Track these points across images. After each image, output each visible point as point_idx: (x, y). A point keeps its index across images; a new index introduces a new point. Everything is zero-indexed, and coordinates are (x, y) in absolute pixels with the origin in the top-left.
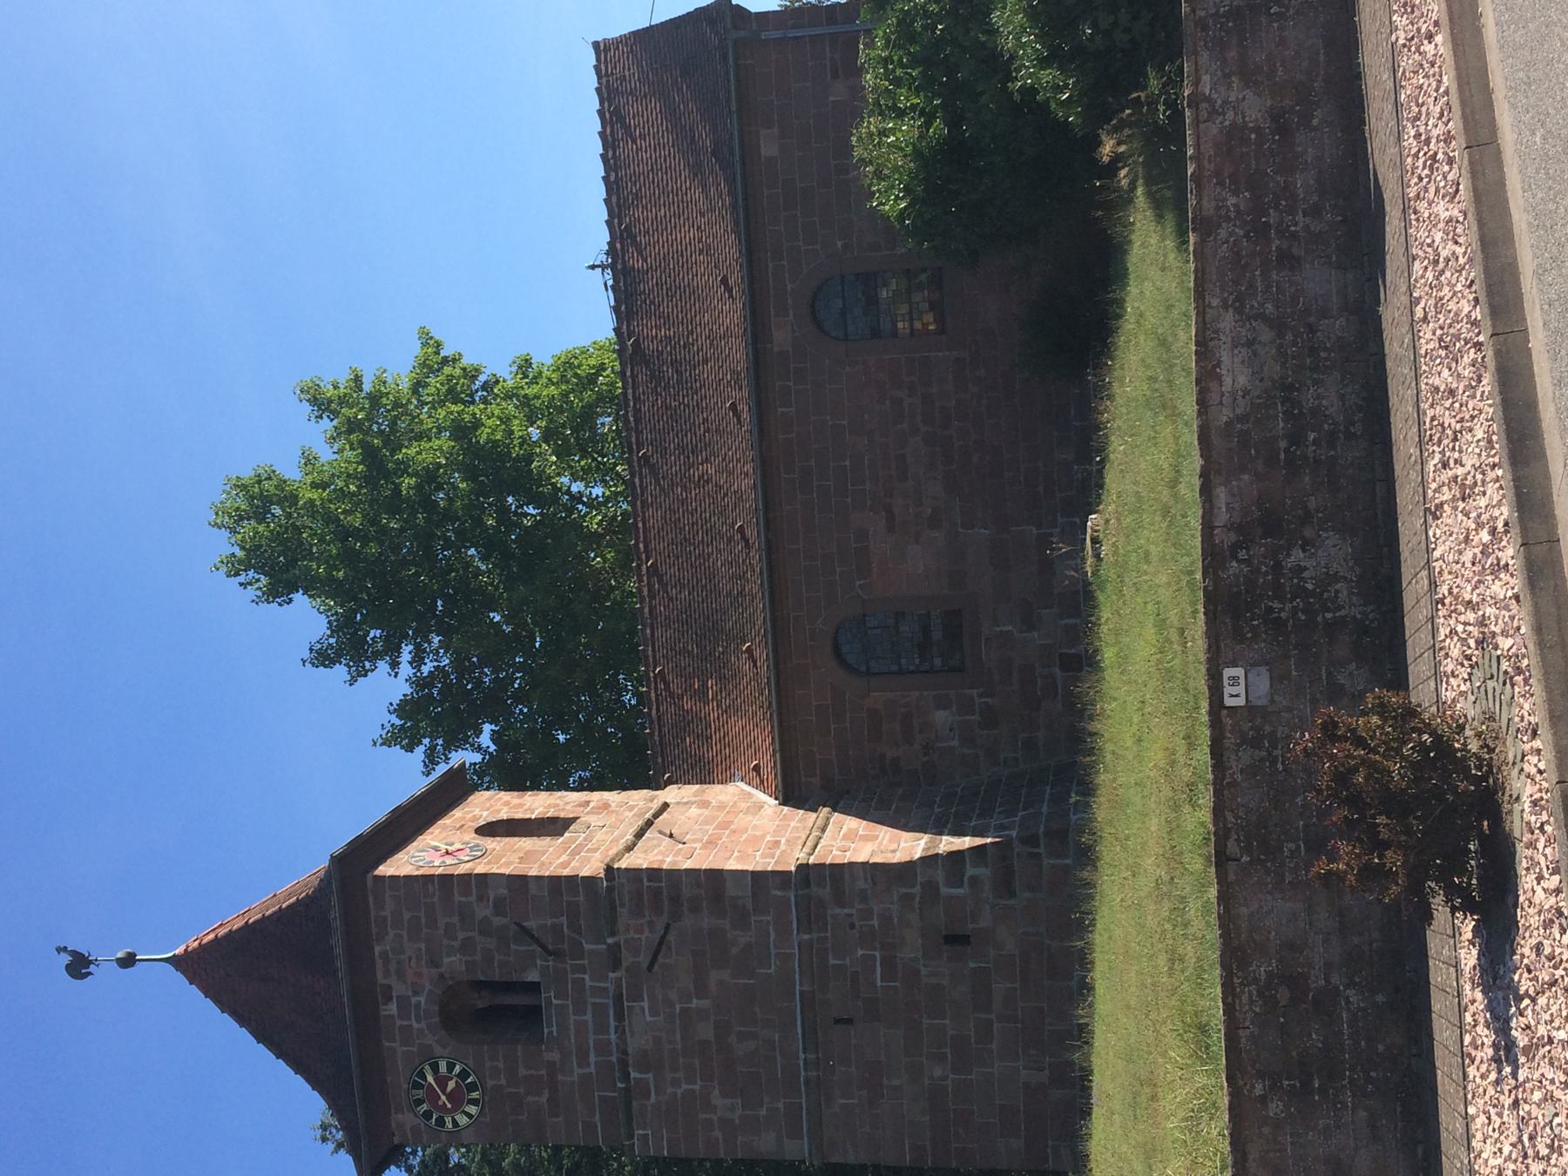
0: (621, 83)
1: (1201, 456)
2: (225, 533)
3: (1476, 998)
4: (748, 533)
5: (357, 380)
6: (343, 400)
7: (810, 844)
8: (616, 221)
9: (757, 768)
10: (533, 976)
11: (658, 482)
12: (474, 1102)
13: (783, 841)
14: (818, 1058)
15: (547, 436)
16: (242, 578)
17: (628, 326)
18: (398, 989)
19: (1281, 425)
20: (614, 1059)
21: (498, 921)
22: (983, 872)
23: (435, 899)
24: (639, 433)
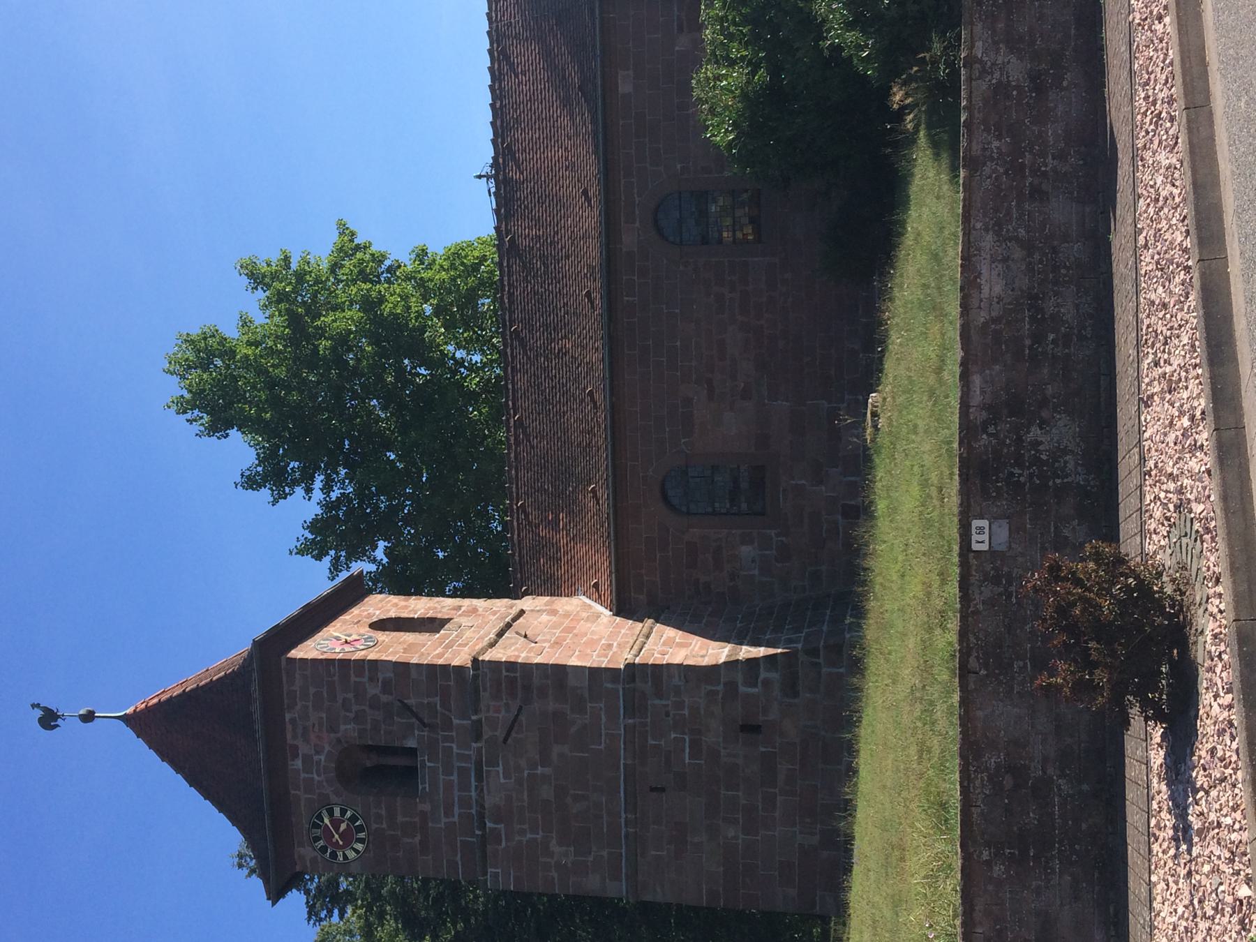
0: (508, 29)
1: (962, 349)
2: (176, 379)
3: (1161, 789)
4: (596, 396)
5: (286, 260)
6: (275, 276)
7: (636, 647)
8: (500, 140)
9: (596, 586)
10: (411, 743)
11: (525, 353)
12: (361, 841)
13: (615, 644)
14: (636, 818)
15: (438, 311)
16: (189, 416)
17: (506, 225)
18: (304, 749)
19: (1027, 327)
20: (473, 812)
21: (385, 698)
22: (774, 676)
23: (336, 678)
24: (511, 312)
